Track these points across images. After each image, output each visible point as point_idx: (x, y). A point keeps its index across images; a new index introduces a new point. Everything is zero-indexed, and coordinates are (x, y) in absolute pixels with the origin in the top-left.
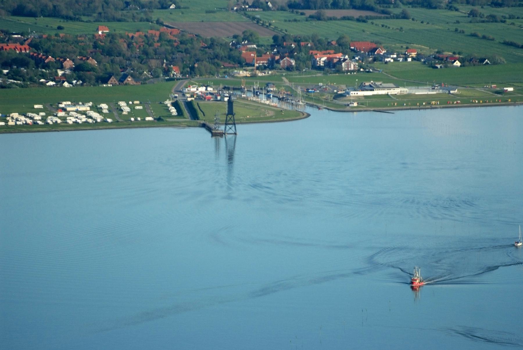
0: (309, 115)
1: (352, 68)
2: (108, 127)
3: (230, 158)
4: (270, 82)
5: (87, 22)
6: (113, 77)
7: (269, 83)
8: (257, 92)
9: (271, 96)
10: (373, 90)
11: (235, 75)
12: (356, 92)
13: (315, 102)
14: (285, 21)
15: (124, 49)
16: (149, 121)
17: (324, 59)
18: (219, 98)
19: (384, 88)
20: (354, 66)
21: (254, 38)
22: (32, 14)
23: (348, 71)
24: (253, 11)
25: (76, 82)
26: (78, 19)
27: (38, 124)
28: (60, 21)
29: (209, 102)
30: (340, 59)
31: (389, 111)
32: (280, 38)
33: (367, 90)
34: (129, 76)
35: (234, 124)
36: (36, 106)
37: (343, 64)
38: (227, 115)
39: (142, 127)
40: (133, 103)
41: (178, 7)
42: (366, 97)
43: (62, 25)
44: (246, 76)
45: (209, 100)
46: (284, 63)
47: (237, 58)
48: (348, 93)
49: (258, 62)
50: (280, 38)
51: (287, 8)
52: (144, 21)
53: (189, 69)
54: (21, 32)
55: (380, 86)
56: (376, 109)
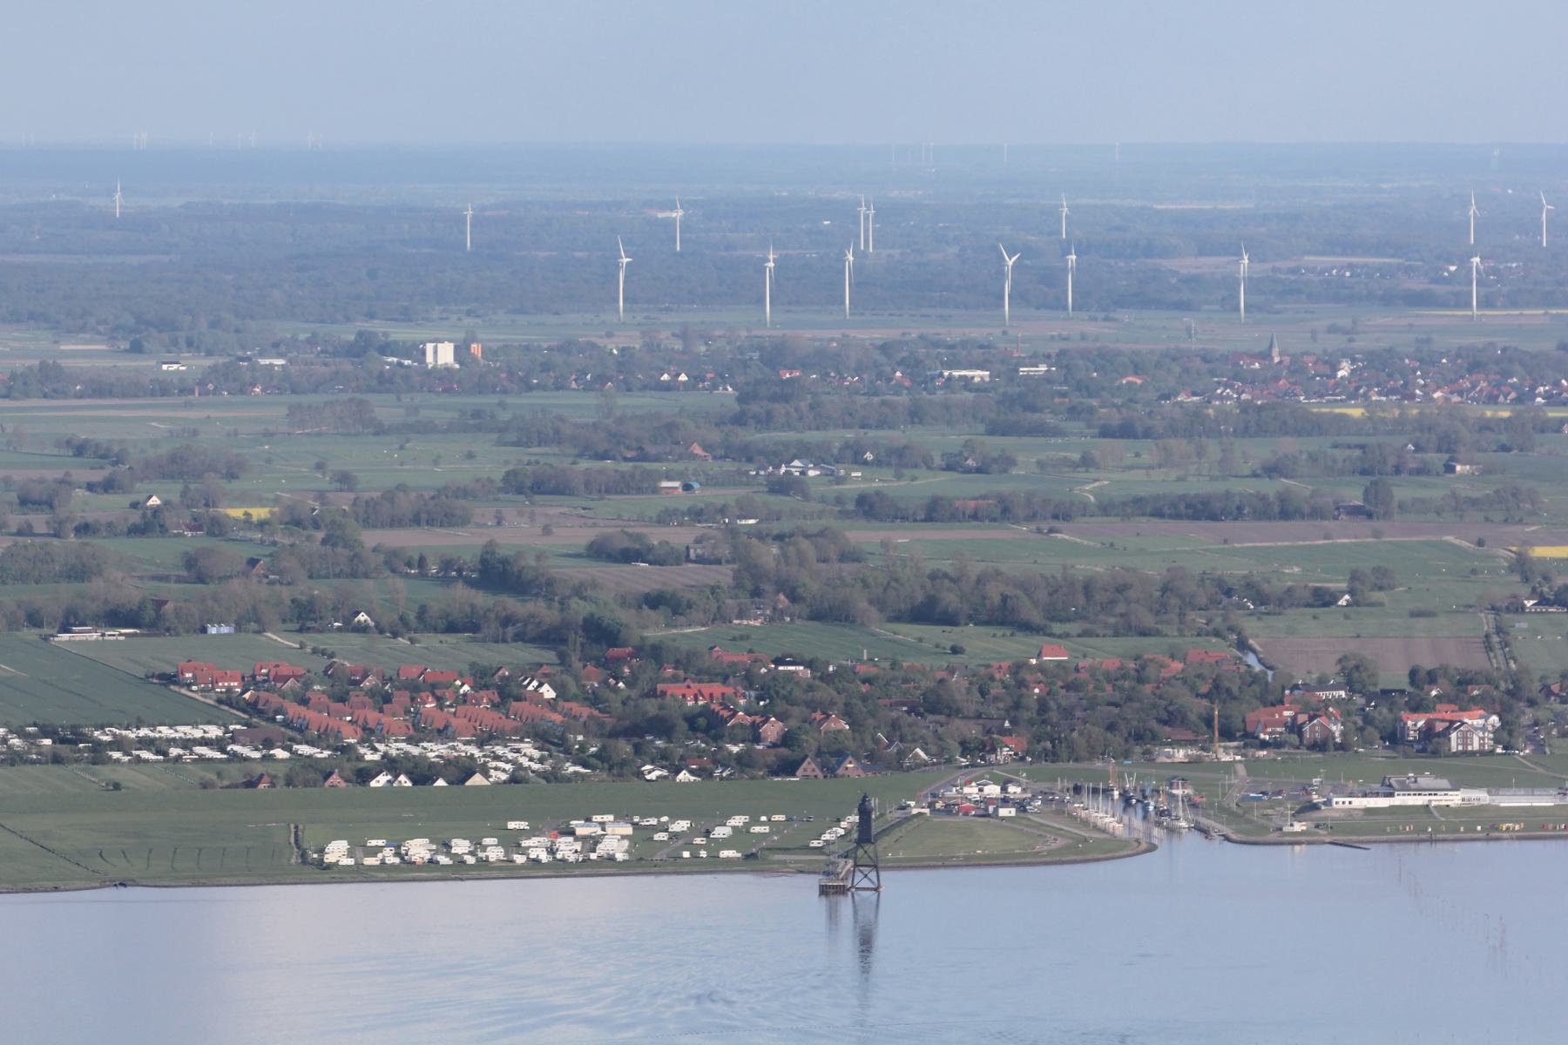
0: (1152, 848)
1: (1476, 746)
3: (866, 942)
5: (1060, 637)
10: (1391, 795)
12: (1347, 800)
15: (958, 697)
16: (728, 859)
18: (991, 809)
19: (1420, 791)
21: (1364, 675)
22: (949, 620)
23: (1465, 753)
33: (1377, 795)
35: (876, 867)
36: (512, 825)
37: (1453, 736)
39: (682, 873)
45: (966, 814)
46: (1312, 731)
48: (1328, 803)
50: (1422, 674)
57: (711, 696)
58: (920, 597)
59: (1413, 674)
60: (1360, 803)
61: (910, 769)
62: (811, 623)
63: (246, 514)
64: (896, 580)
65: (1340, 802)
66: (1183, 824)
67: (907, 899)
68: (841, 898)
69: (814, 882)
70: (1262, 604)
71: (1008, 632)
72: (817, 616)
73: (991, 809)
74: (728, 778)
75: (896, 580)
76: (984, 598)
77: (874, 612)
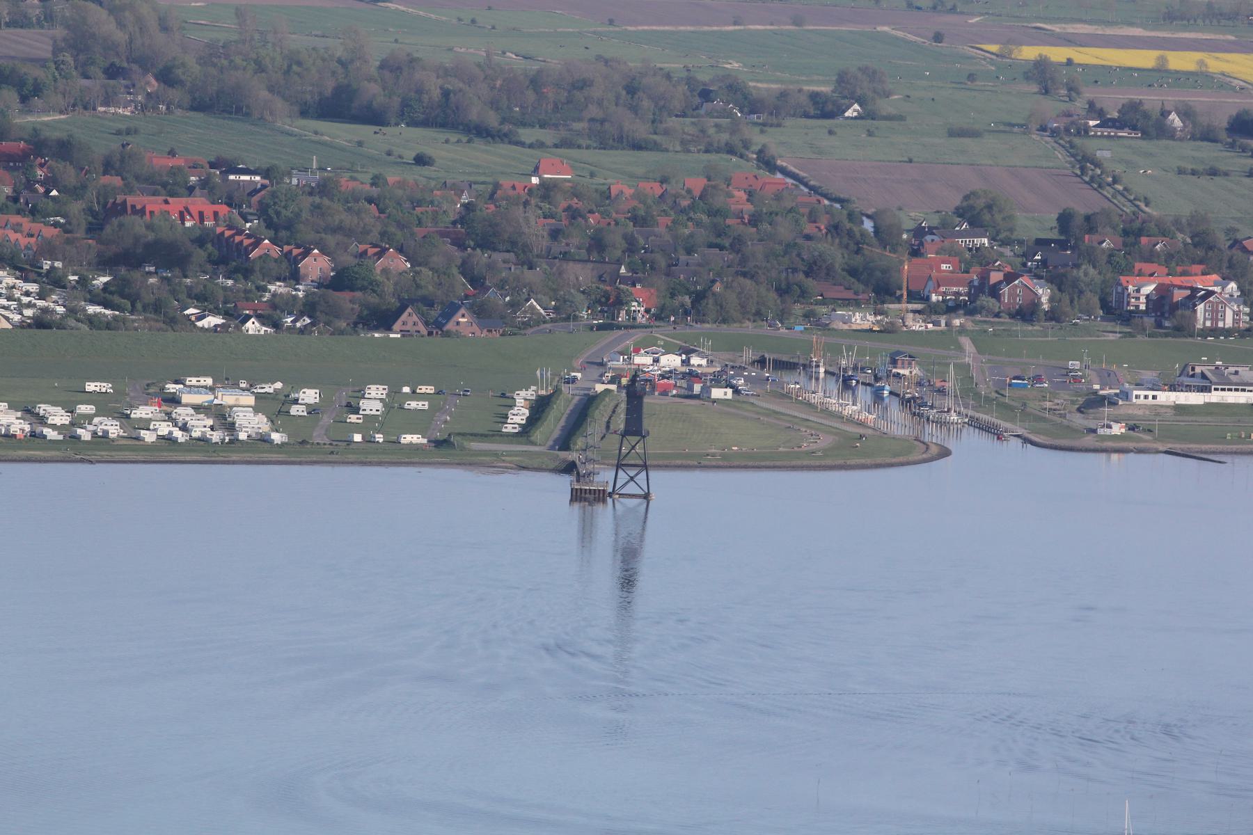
2: (266, 457)
3: (628, 582)
4: (902, 348)
5: (531, 146)
6: (409, 310)
7: (899, 353)
8: (850, 378)
9: (886, 393)
11: (834, 326)
12: (1151, 393)
13: (997, 413)
14: (1181, 171)
17: (1148, 289)
18: (697, 388)
20: (1236, 313)
21: (998, 217)
22: (374, 117)
23: (1215, 331)
24: (1109, 137)
25: (294, 322)
26: (506, 135)
27: (45, 437)
28: (447, 141)
29: (668, 399)
30: (1194, 290)
31: (1211, 457)
32: (1078, 221)
33: (1189, 388)
34: (462, 311)
35: (645, 467)
37: (1200, 308)
38: (623, 436)
39: (370, 464)
40: (414, 392)
41: (868, 115)
42: (1180, 409)
43: (428, 151)
44: (871, 330)
45: (664, 393)
46: (1012, 295)
47: (878, 274)
48: (1126, 395)
49: (943, 289)
50: (1078, 221)
51: (1223, 135)
52: (718, 151)
53: (687, 300)
54: (265, 166)
55: (1233, 378)
56: (1178, 447)
57: (201, 214)
58: (329, 86)
59: (1065, 220)
60: (1167, 398)
61: (526, 325)
62: (192, 114)
63: (1201, 63)
64: (299, 64)
65: (1141, 397)
66: (954, 417)
67: (691, 511)
68: (599, 508)
69: (565, 483)
70: (752, 112)
71: (465, 139)
72: (199, 106)
73: (697, 388)
74: (302, 331)
75: (299, 64)
76: (420, 91)
77: (279, 104)
